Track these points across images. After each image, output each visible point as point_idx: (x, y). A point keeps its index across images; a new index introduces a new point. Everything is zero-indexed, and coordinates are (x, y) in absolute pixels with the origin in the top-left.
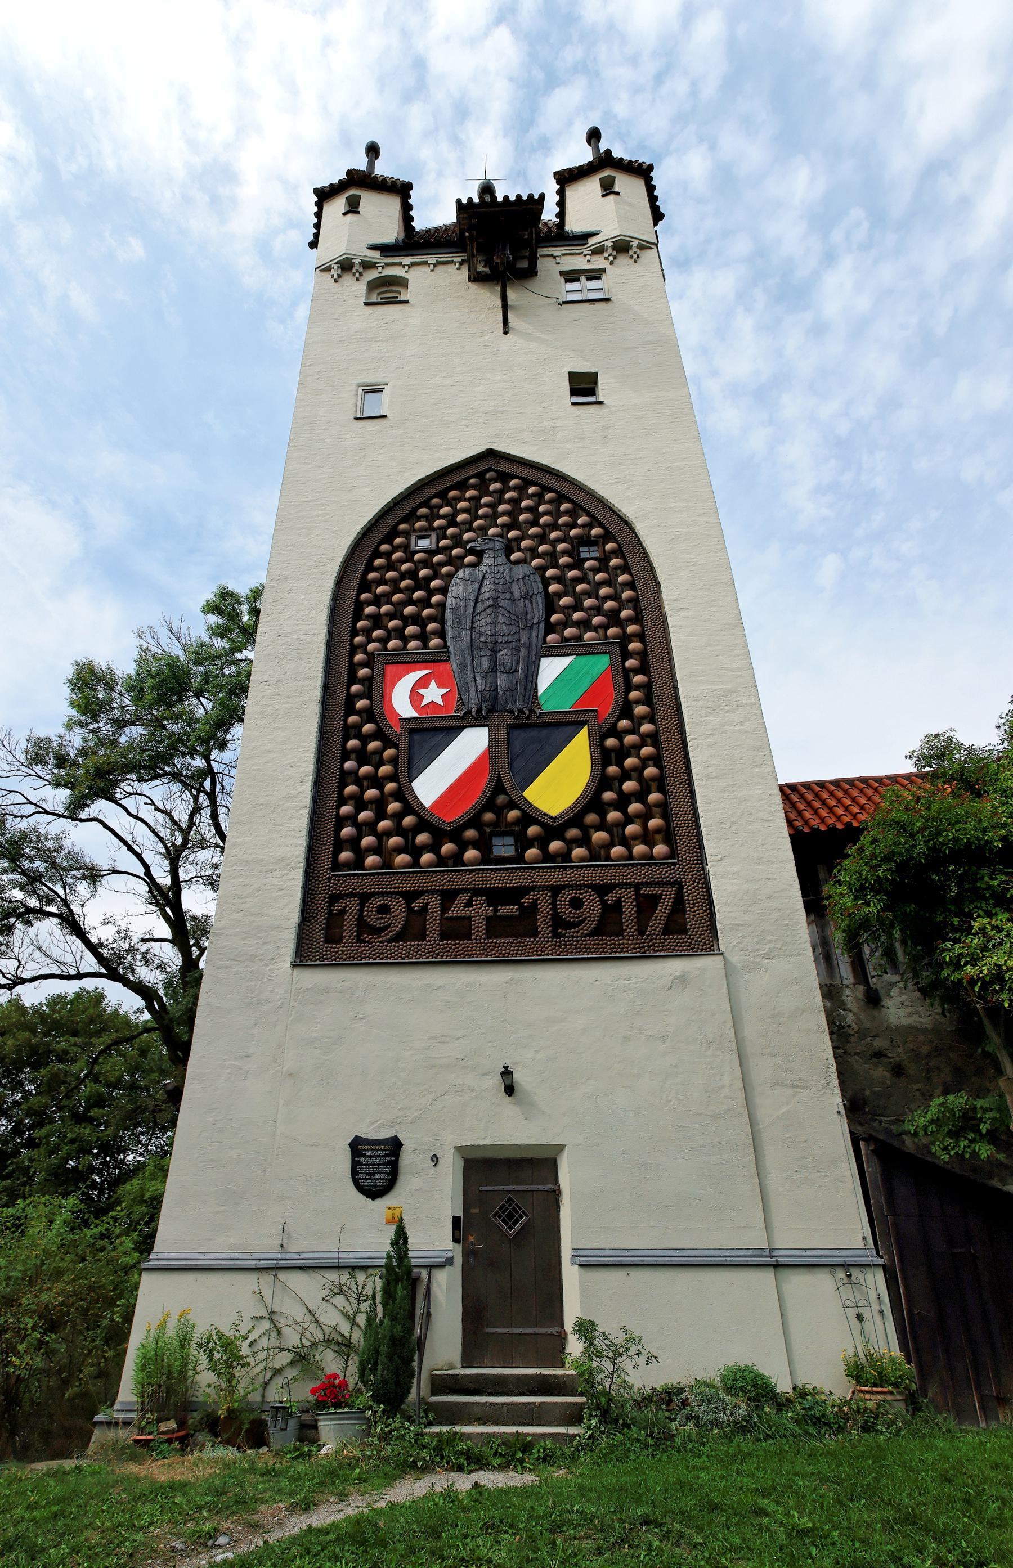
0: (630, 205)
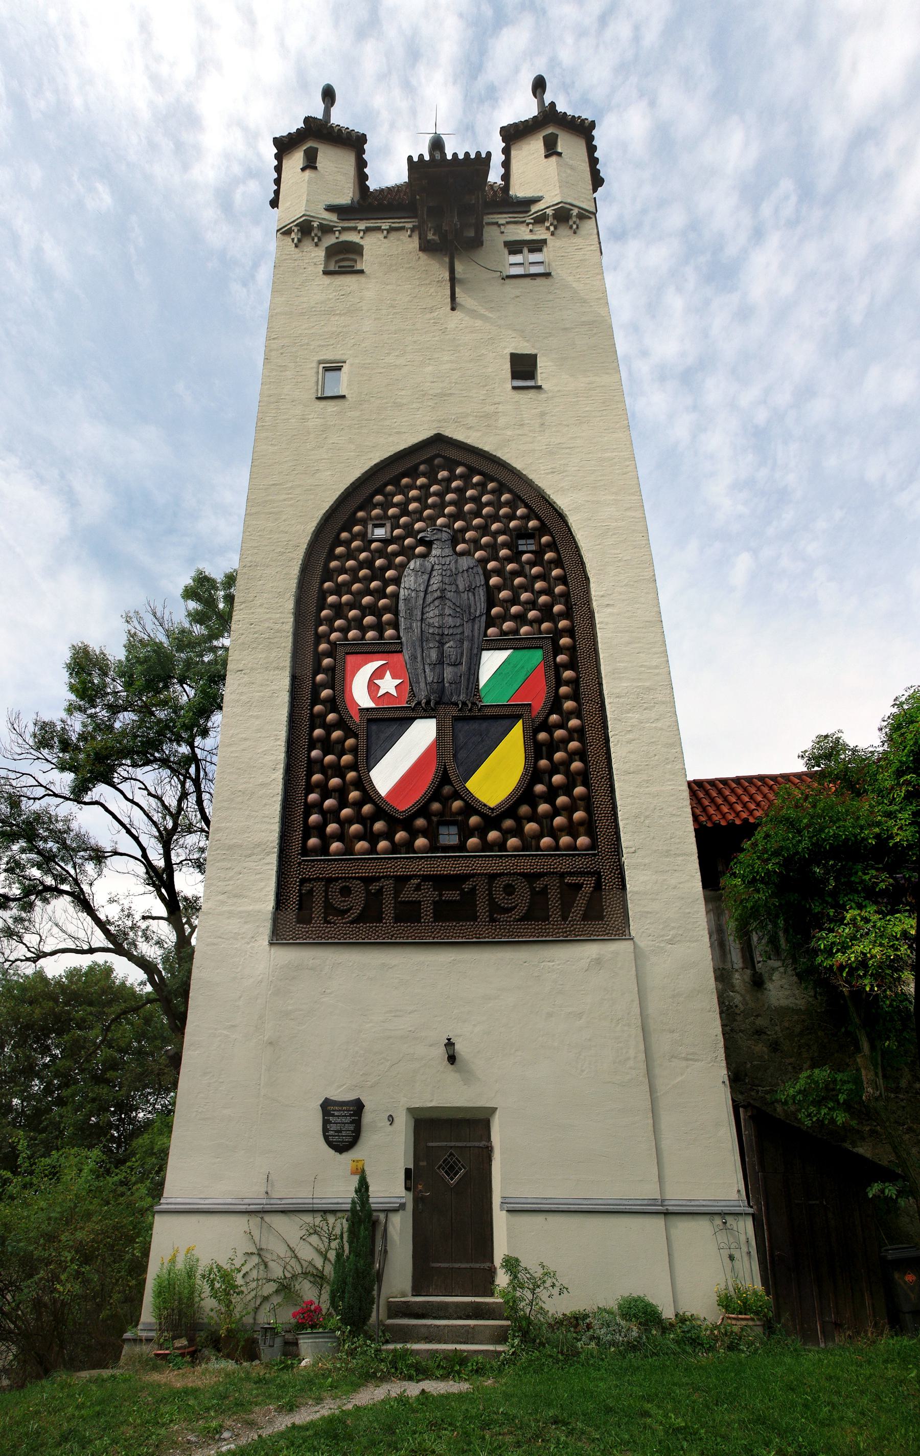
0: (572, 168)
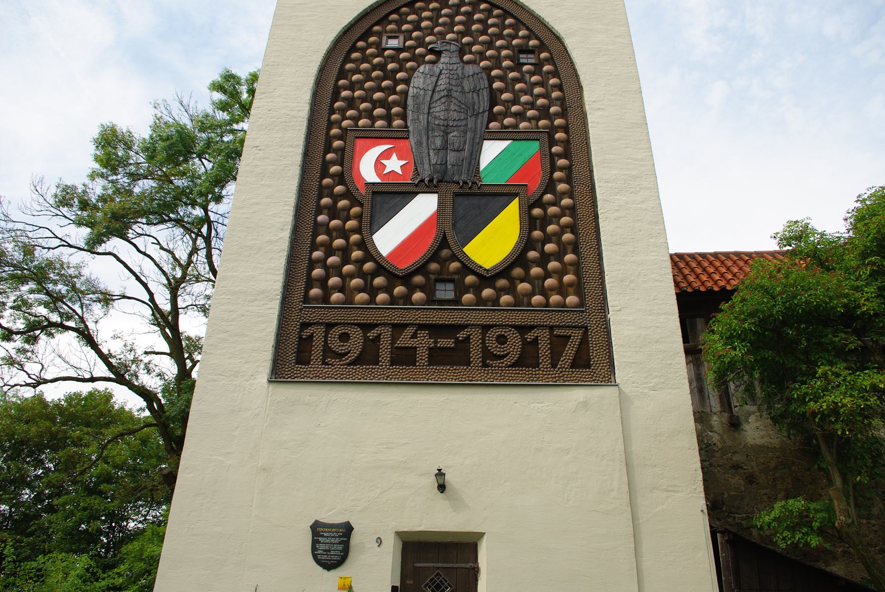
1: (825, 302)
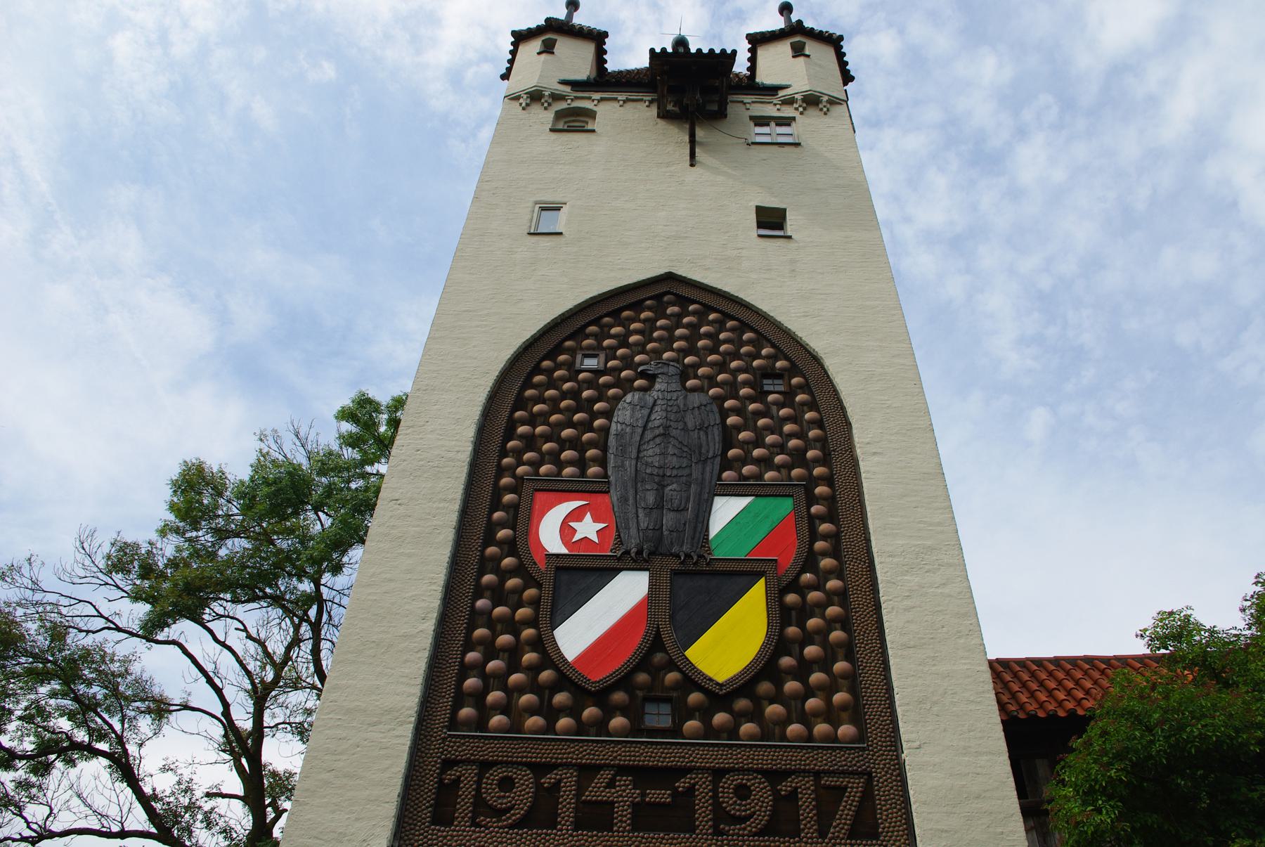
0: (820, 66)
1: (1229, 736)
